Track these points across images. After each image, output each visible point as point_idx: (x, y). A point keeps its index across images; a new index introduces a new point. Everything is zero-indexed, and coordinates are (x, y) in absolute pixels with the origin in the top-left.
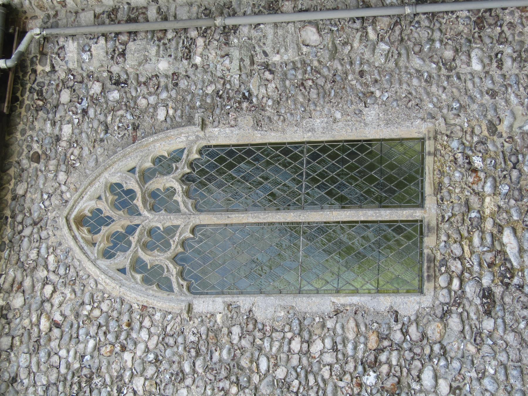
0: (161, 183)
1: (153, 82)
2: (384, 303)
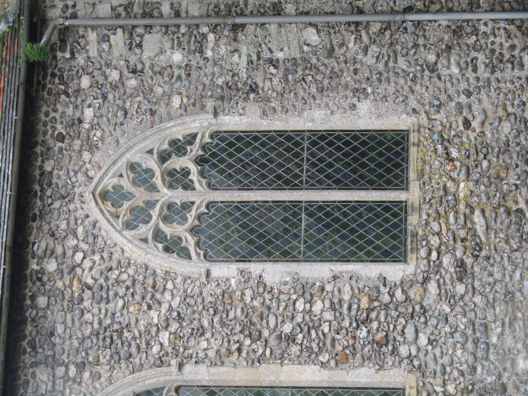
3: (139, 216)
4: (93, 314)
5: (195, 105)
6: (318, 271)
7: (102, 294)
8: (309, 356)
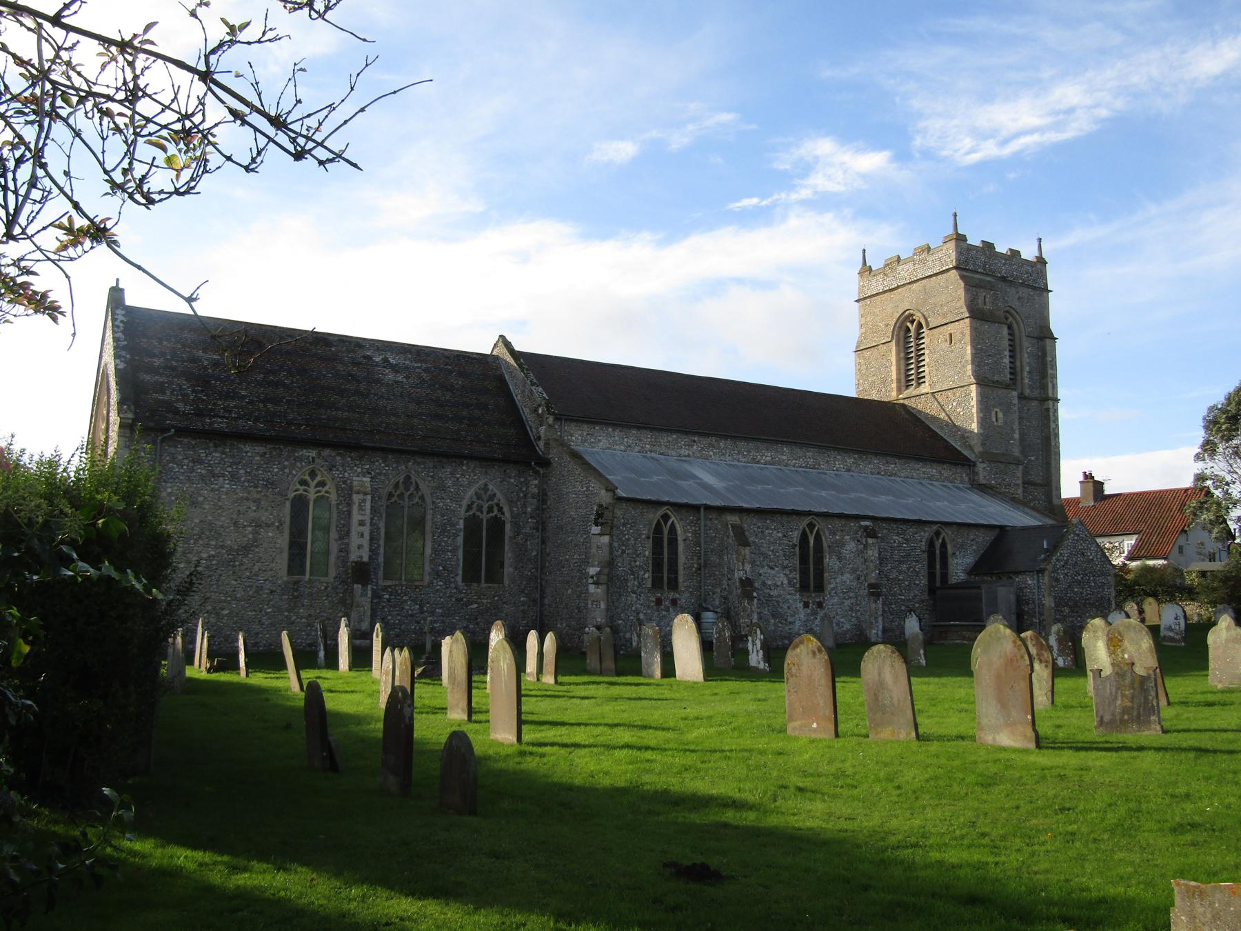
0: (495, 509)
1: (525, 506)
2: (460, 572)
3: (479, 497)
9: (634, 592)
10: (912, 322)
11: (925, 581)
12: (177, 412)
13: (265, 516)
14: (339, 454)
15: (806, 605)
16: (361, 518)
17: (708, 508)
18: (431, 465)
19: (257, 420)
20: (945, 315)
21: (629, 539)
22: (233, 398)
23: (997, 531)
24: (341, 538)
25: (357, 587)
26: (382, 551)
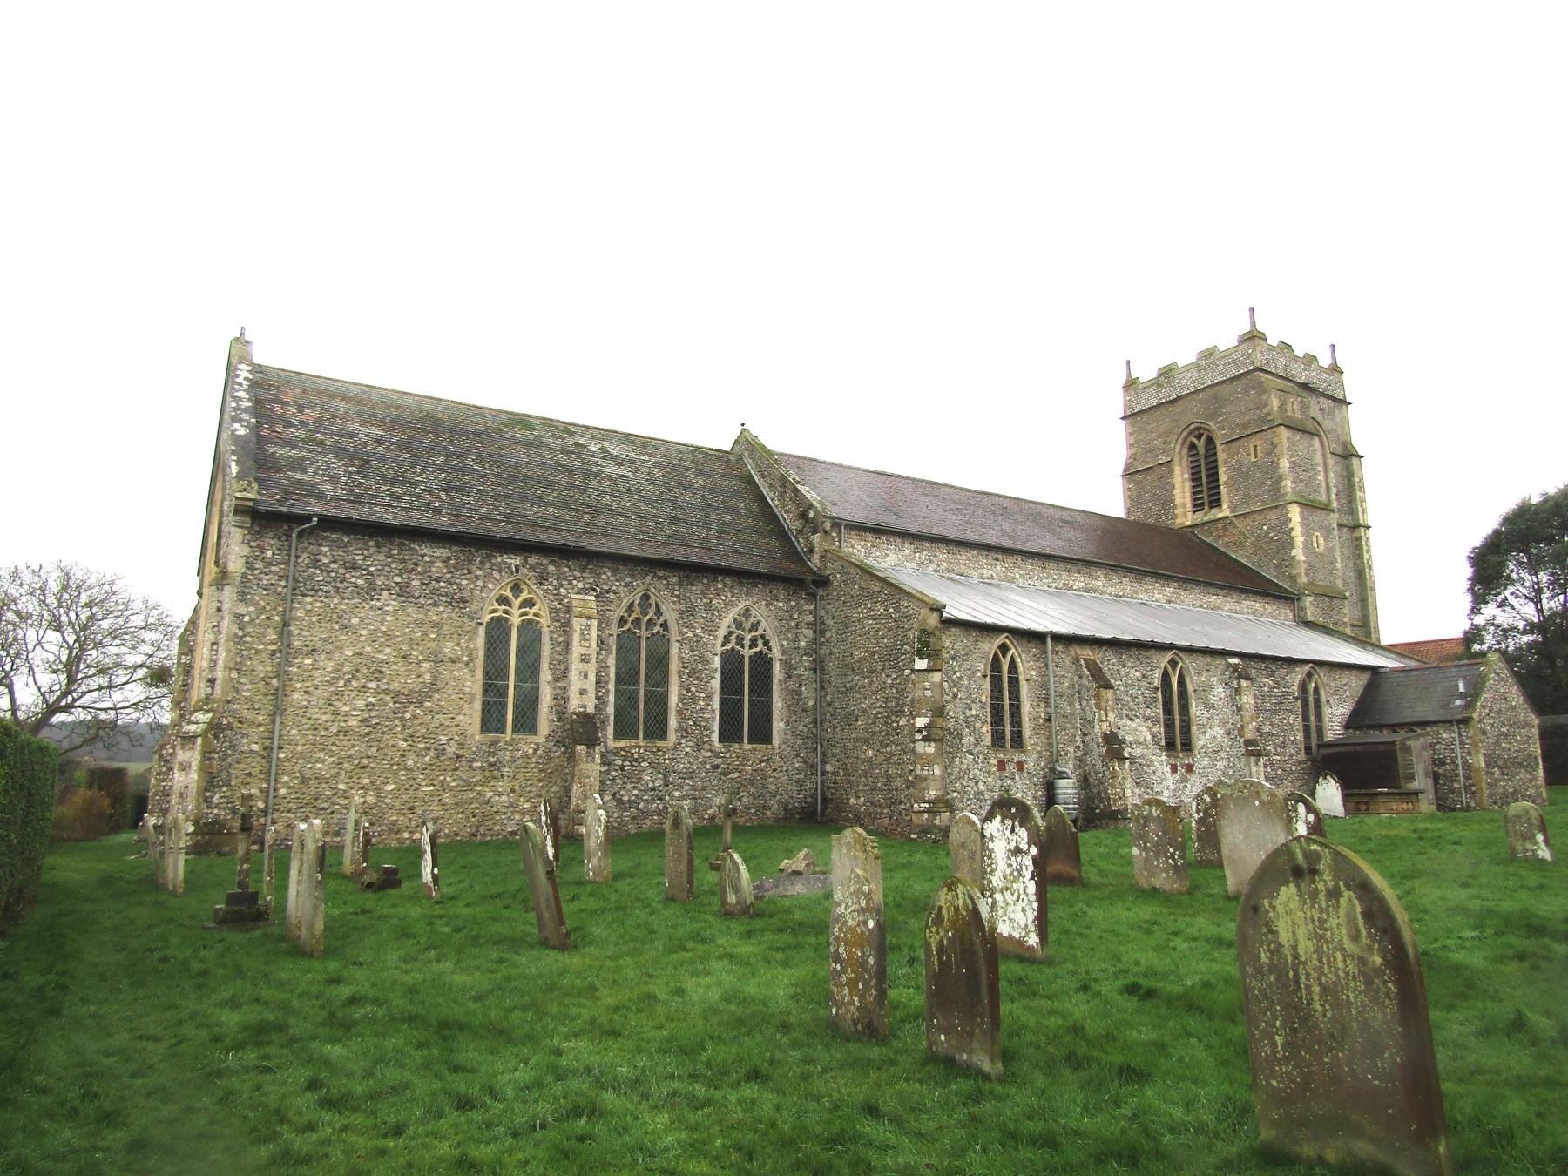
0: (760, 642)
1: (797, 639)
3: (739, 625)
4: (700, 603)
5: (784, 651)
6: (716, 704)
7: (708, 607)
8: (682, 698)
9: (970, 753)
10: (1199, 437)
11: (1300, 737)
12: (321, 496)
13: (448, 649)
14: (552, 562)
15: (1174, 769)
16: (583, 651)
17: (1058, 638)
18: (675, 580)
19: (437, 511)
20: (1245, 426)
21: (960, 678)
22: (403, 483)
23: (1364, 678)
24: (556, 679)
25: (581, 749)
26: (611, 698)
